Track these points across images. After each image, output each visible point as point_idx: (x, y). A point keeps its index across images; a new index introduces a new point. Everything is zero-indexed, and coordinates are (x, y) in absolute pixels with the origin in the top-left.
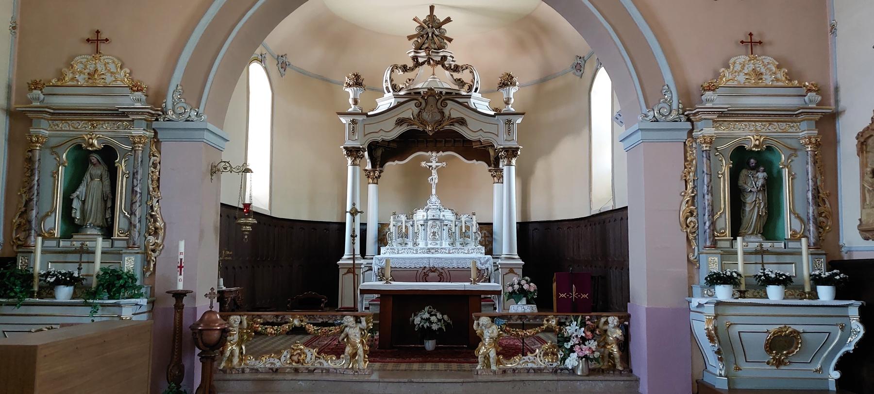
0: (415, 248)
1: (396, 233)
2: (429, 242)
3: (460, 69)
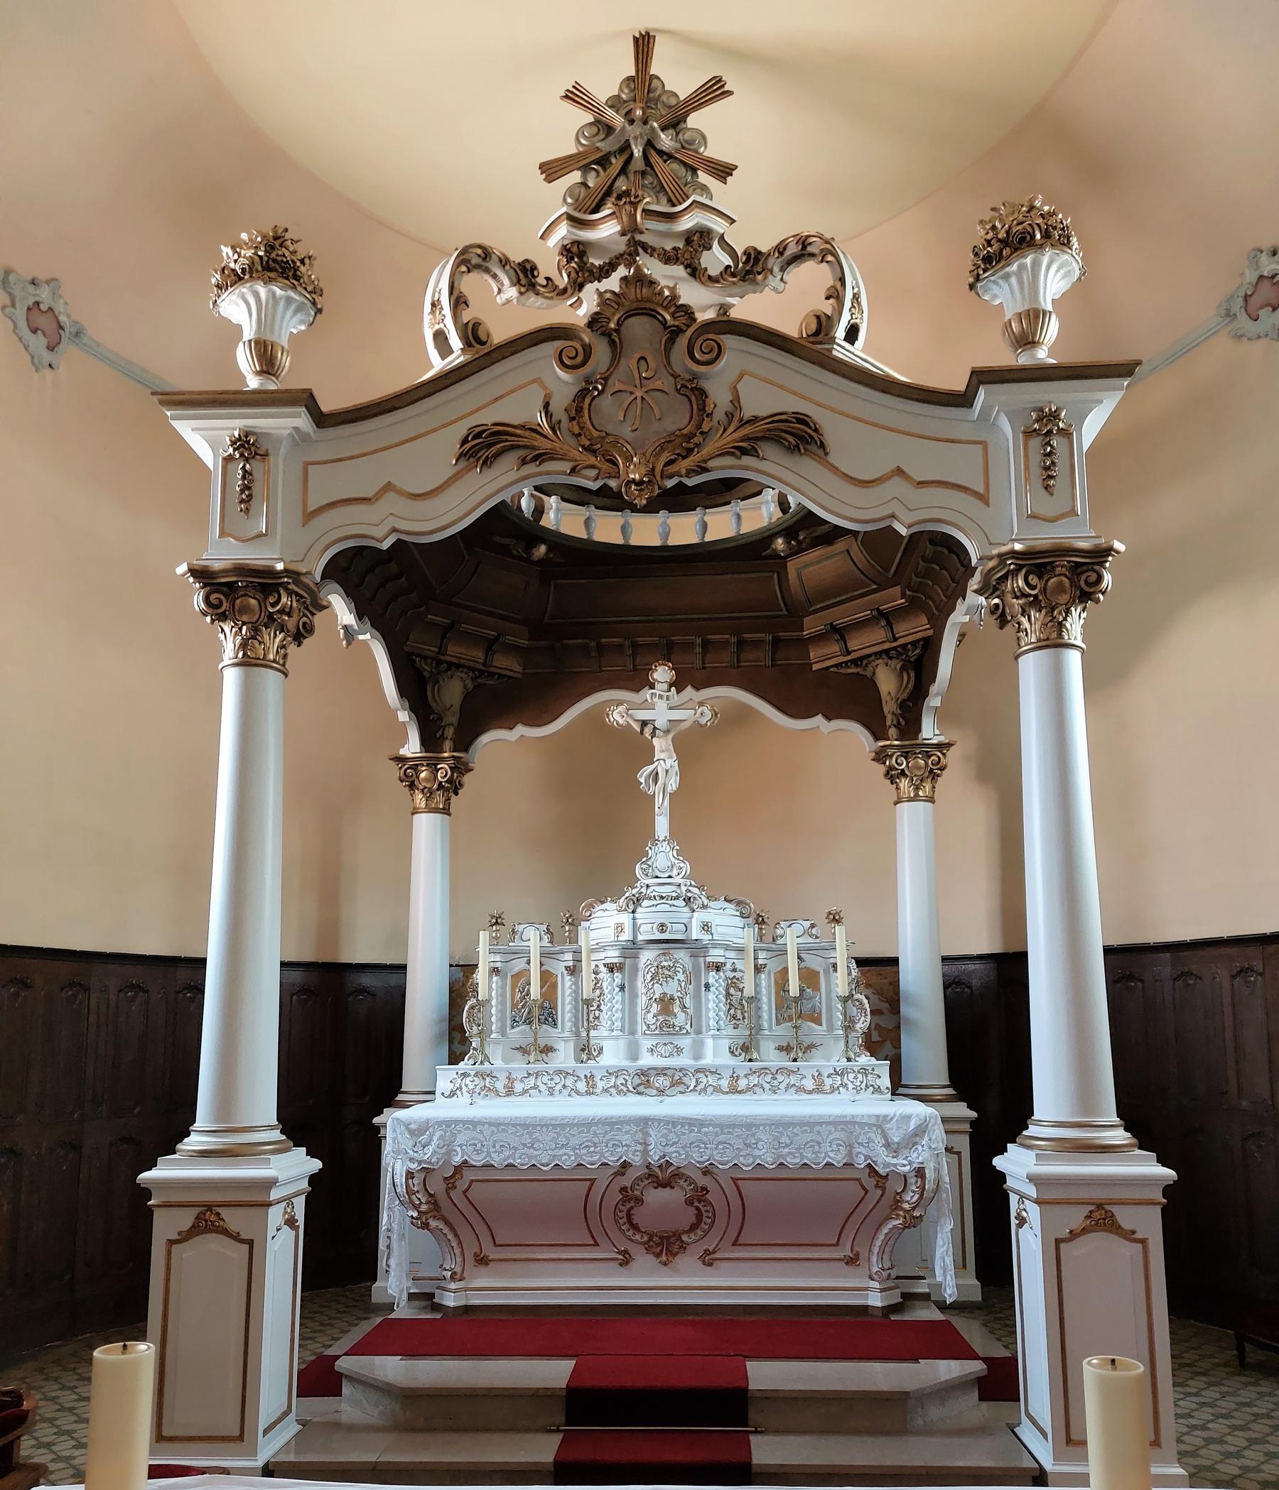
0: (583, 1070)
1: (502, 1003)
2: (646, 1043)
3: (771, 261)
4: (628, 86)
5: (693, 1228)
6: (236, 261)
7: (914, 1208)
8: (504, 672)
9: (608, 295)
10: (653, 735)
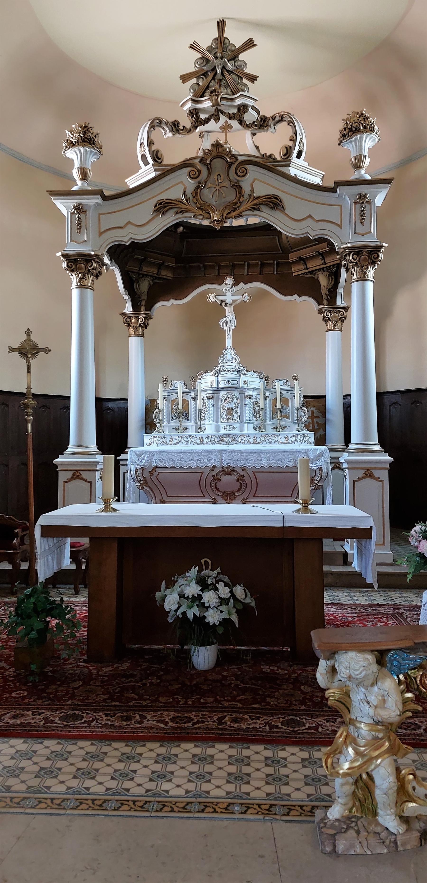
1: (168, 411)
2: (222, 426)
3: (270, 122)
4: (215, 42)
5: (239, 490)
6: (72, 138)
7: (318, 482)
8: (165, 277)
9: (207, 151)
10: (226, 306)
